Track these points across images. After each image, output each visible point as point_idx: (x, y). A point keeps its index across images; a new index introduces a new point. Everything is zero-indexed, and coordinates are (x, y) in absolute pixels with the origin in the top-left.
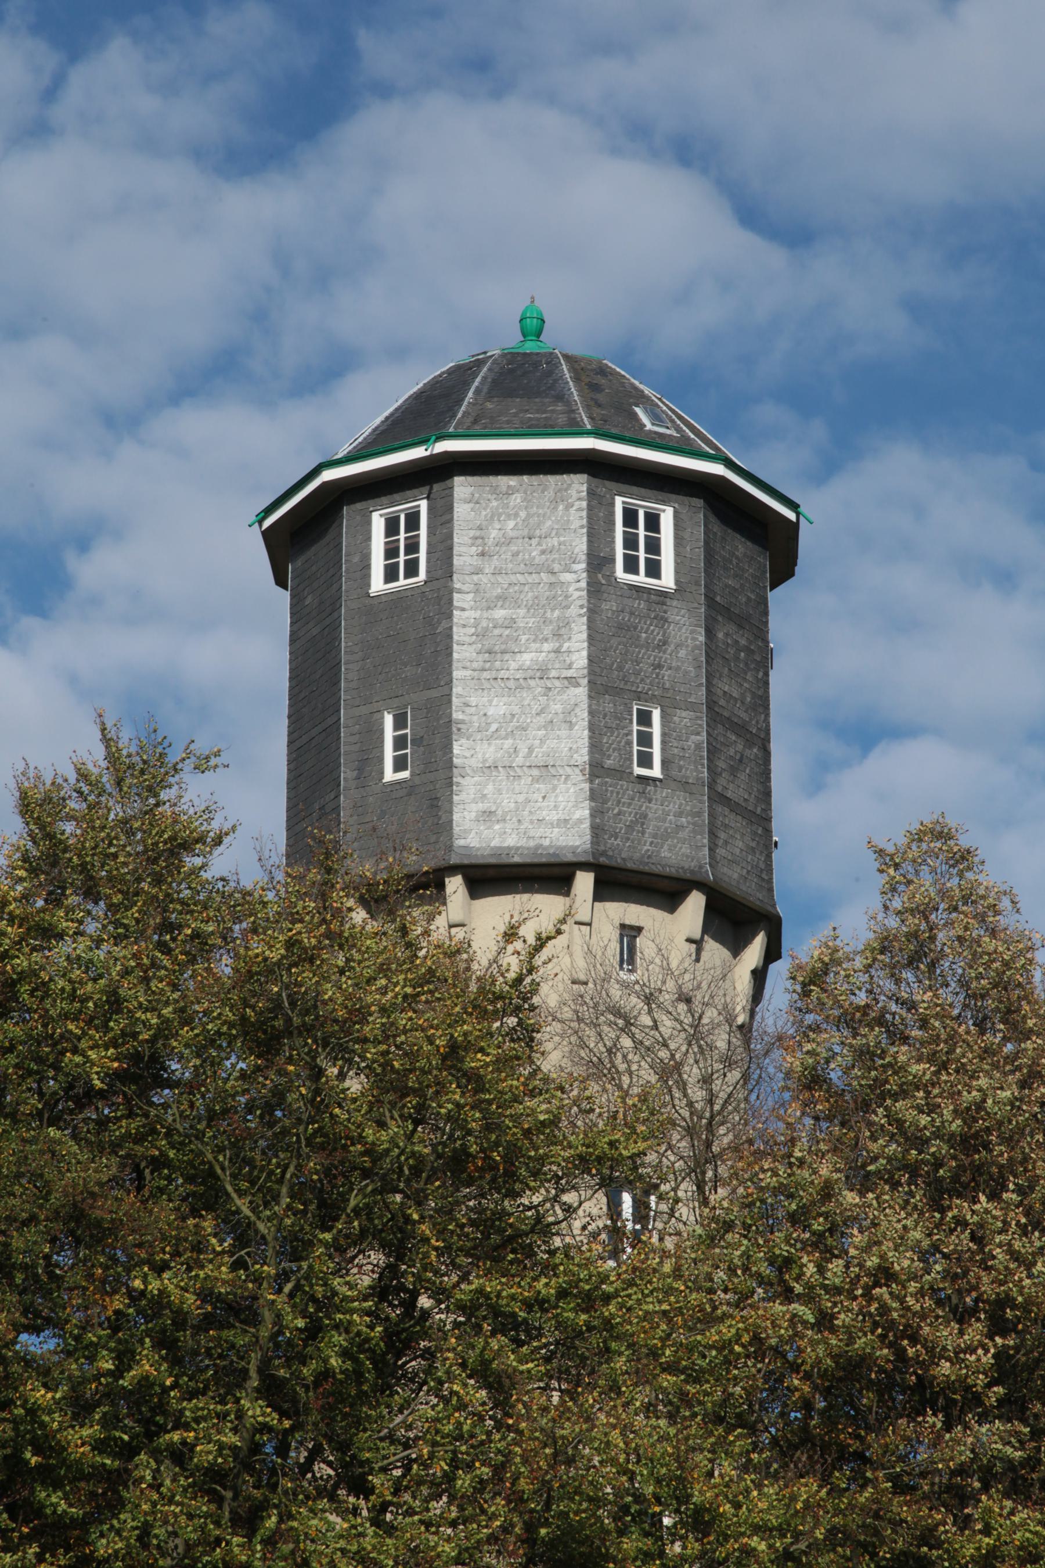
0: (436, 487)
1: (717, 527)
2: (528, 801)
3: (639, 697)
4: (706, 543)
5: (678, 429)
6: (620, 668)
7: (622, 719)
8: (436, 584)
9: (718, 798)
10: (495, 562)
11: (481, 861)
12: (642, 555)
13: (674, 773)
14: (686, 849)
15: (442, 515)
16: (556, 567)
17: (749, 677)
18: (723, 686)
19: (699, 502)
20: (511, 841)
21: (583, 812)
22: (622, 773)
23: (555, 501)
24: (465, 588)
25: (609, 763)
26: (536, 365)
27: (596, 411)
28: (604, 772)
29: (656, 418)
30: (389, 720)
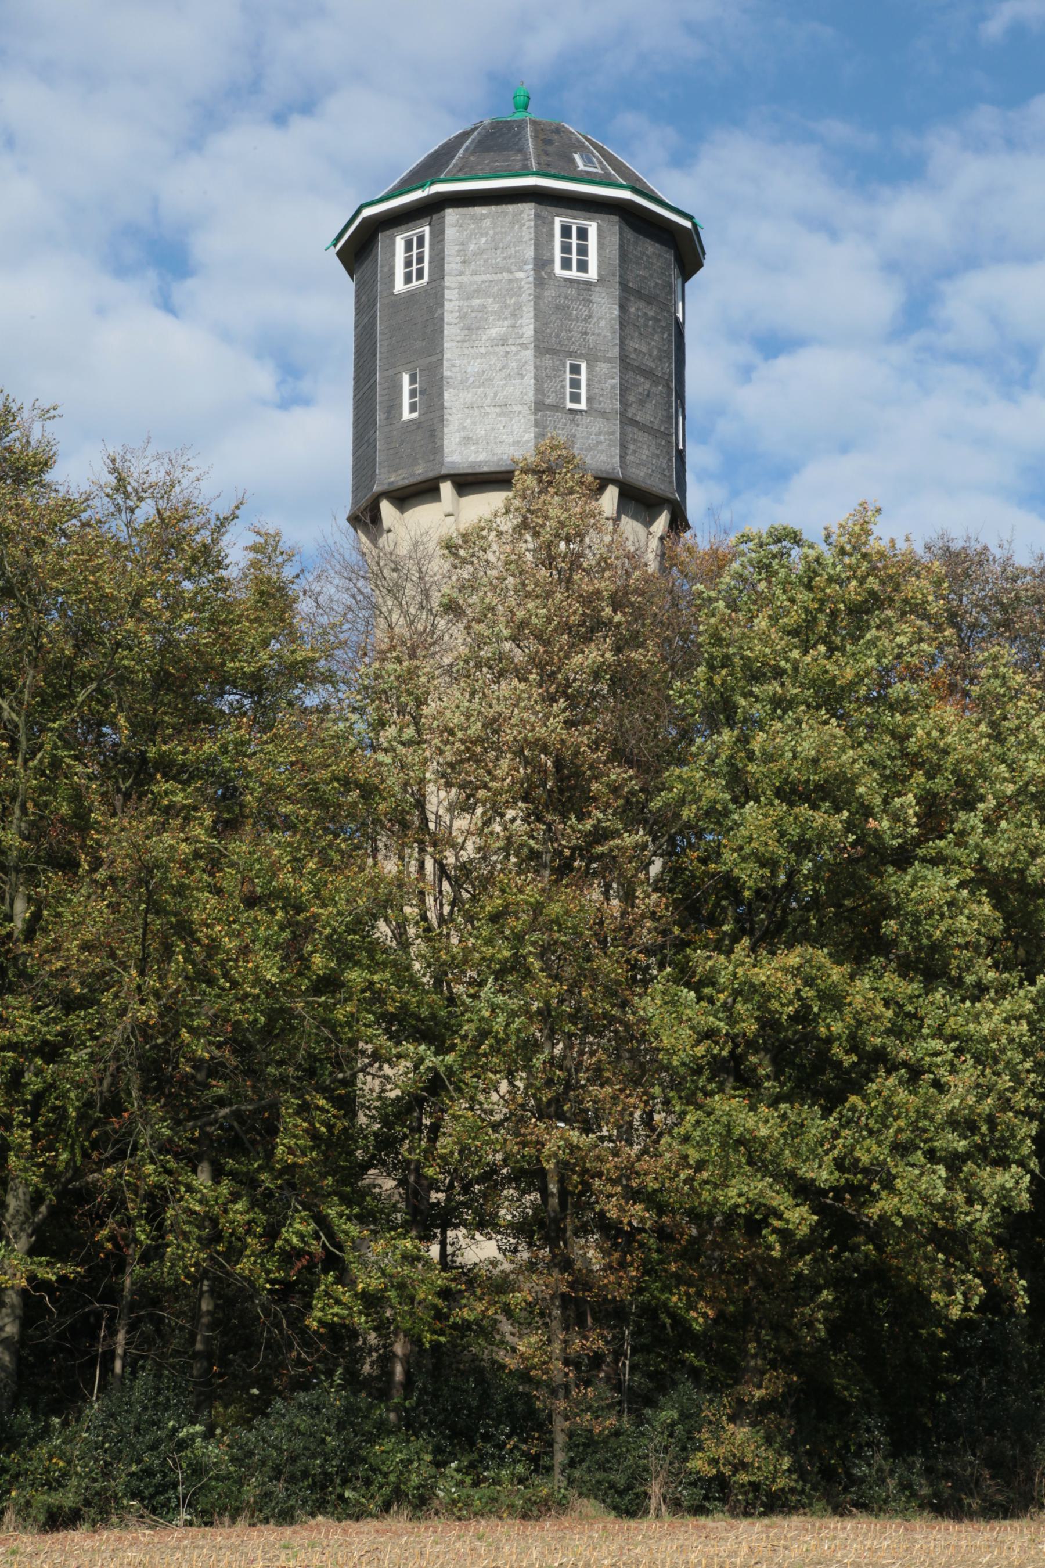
0: (435, 217)
1: (630, 235)
2: (493, 429)
3: (570, 355)
4: (621, 246)
5: (603, 168)
6: (557, 336)
7: (558, 371)
8: (433, 284)
9: (627, 421)
10: (473, 267)
11: (461, 471)
12: (574, 257)
13: (596, 405)
14: (603, 458)
15: (438, 236)
16: (513, 268)
17: (656, 337)
18: (634, 344)
19: (615, 218)
20: (482, 457)
21: (530, 436)
22: (558, 408)
23: (512, 223)
24: (453, 286)
25: (548, 401)
26: (510, 128)
27: (544, 158)
28: (543, 406)
29: (588, 162)
30: (406, 378)
